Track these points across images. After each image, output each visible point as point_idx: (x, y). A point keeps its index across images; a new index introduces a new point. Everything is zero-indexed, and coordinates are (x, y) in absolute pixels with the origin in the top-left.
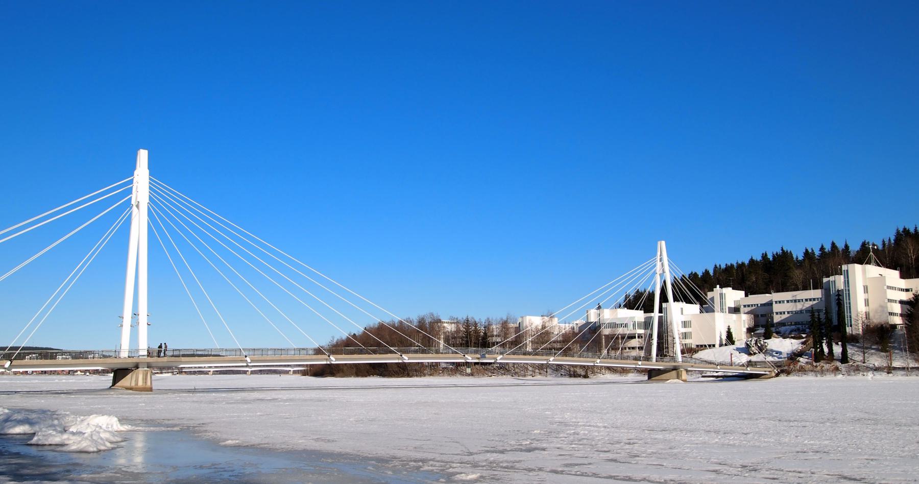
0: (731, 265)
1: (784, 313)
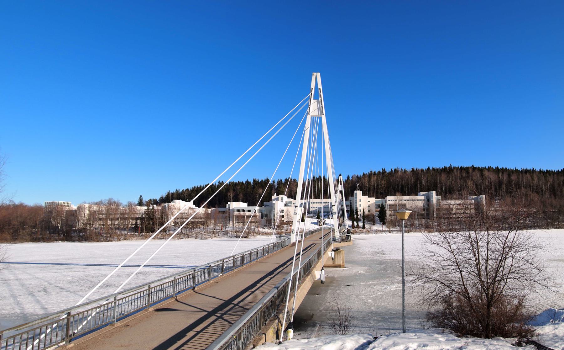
0: (247, 181)
1: (315, 208)
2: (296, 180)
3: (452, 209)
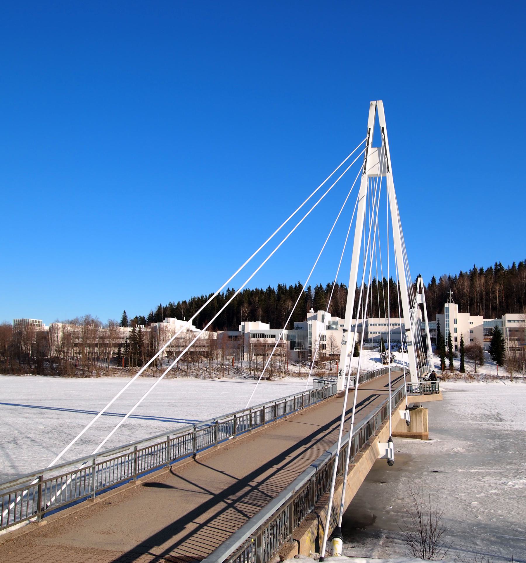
0: (269, 288)
1: (376, 333)
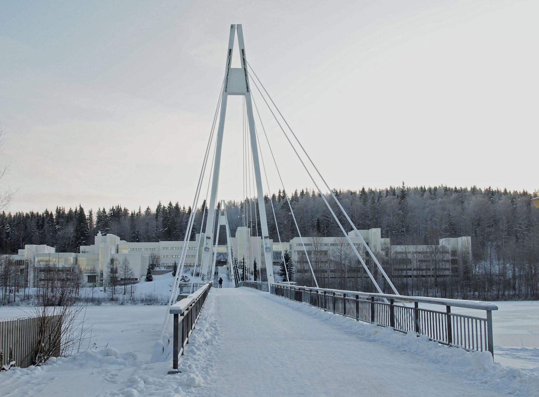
0: (47, 212)
2: (127, 210)
3: (408, 261)
